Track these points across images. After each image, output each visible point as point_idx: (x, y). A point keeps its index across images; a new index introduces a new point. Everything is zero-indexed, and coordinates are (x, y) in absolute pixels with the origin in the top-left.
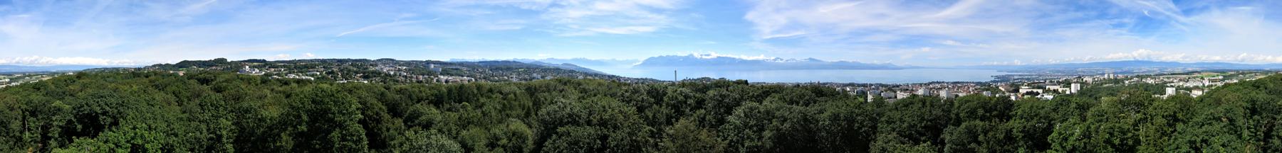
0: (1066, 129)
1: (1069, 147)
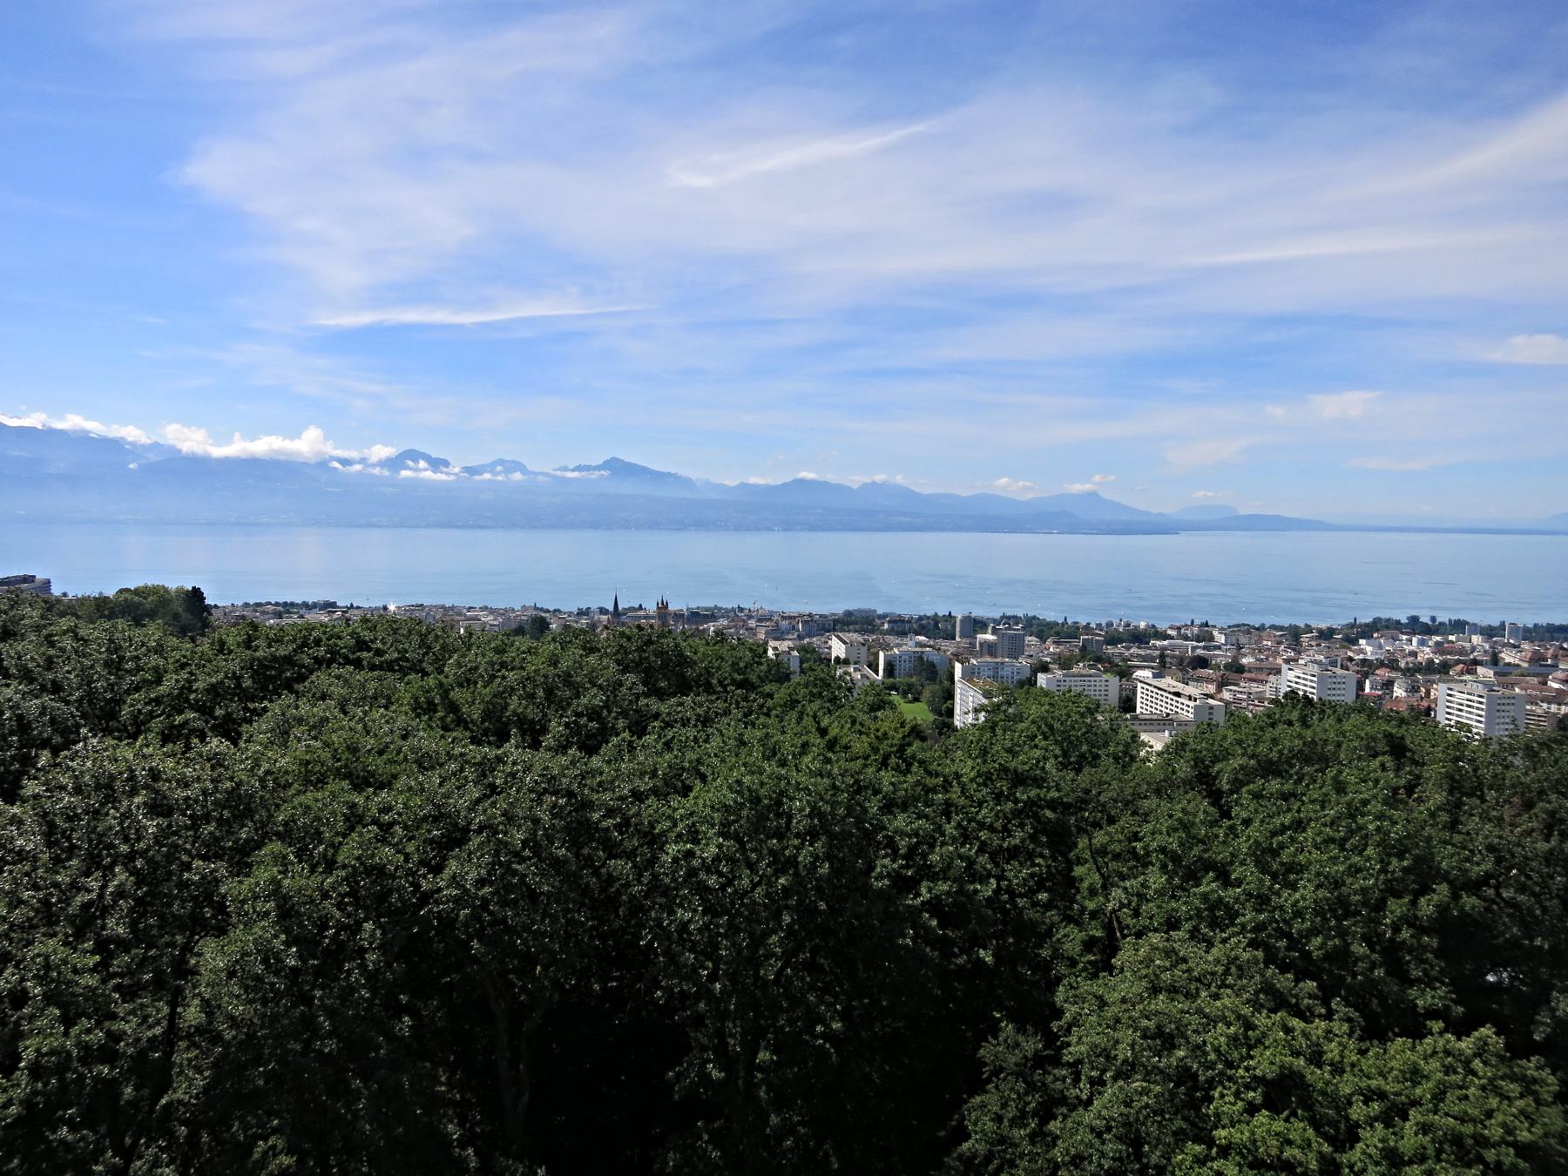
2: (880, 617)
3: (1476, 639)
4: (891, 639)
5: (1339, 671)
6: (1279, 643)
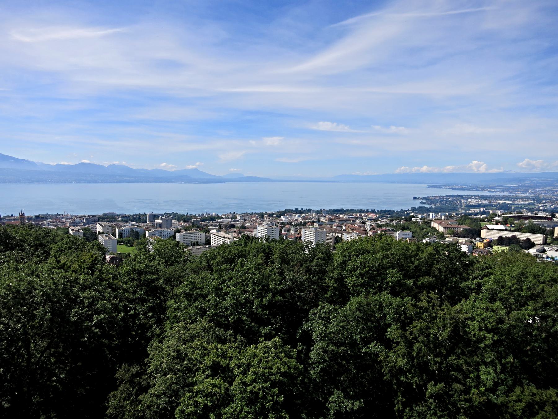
2: (118, 215)
3: (314, 215)
4: (122, 224)
5: (274, 227)
6: (257, 218)
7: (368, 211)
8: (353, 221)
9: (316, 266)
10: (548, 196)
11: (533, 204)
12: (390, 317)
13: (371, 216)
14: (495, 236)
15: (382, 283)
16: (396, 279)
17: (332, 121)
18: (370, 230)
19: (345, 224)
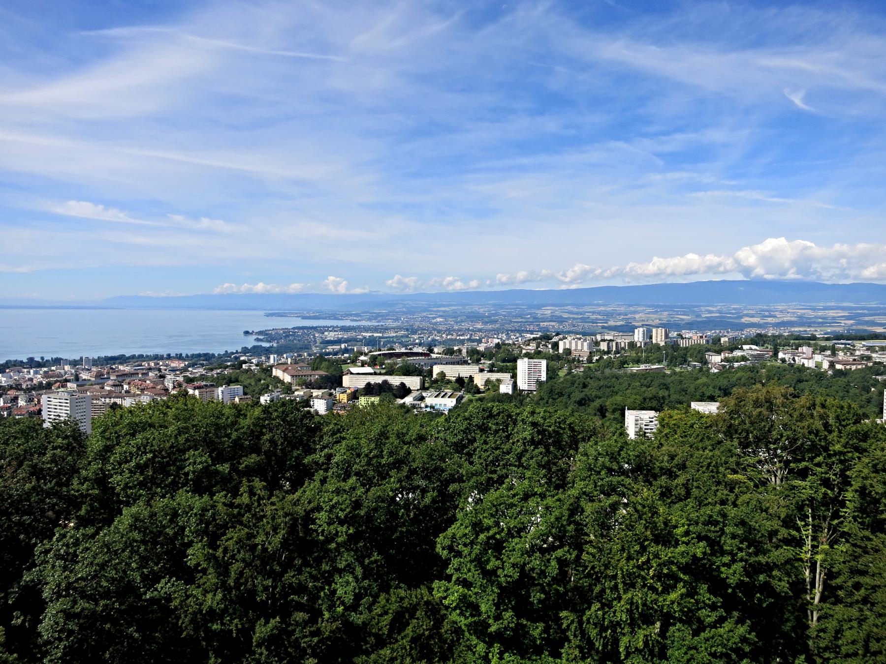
0: (497, 512)
1: (508, 573)
3: (67, 368)
7: (169, 357)
8: (143, 374)
9: (51, 462)
10: (424, 325)
11: (407, 337)
12: (190, 531)
13: (175, 364)
14: (361, 383)
15: (177, 475)
16: (200, 467)
17: (96, 201)
18: (174, 387)
19: (128, 380)
